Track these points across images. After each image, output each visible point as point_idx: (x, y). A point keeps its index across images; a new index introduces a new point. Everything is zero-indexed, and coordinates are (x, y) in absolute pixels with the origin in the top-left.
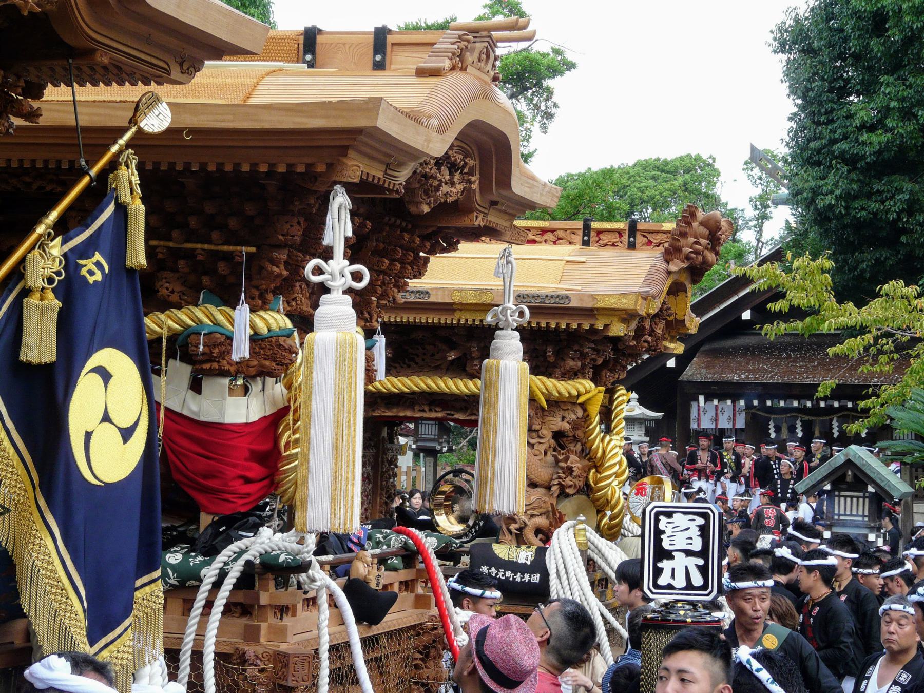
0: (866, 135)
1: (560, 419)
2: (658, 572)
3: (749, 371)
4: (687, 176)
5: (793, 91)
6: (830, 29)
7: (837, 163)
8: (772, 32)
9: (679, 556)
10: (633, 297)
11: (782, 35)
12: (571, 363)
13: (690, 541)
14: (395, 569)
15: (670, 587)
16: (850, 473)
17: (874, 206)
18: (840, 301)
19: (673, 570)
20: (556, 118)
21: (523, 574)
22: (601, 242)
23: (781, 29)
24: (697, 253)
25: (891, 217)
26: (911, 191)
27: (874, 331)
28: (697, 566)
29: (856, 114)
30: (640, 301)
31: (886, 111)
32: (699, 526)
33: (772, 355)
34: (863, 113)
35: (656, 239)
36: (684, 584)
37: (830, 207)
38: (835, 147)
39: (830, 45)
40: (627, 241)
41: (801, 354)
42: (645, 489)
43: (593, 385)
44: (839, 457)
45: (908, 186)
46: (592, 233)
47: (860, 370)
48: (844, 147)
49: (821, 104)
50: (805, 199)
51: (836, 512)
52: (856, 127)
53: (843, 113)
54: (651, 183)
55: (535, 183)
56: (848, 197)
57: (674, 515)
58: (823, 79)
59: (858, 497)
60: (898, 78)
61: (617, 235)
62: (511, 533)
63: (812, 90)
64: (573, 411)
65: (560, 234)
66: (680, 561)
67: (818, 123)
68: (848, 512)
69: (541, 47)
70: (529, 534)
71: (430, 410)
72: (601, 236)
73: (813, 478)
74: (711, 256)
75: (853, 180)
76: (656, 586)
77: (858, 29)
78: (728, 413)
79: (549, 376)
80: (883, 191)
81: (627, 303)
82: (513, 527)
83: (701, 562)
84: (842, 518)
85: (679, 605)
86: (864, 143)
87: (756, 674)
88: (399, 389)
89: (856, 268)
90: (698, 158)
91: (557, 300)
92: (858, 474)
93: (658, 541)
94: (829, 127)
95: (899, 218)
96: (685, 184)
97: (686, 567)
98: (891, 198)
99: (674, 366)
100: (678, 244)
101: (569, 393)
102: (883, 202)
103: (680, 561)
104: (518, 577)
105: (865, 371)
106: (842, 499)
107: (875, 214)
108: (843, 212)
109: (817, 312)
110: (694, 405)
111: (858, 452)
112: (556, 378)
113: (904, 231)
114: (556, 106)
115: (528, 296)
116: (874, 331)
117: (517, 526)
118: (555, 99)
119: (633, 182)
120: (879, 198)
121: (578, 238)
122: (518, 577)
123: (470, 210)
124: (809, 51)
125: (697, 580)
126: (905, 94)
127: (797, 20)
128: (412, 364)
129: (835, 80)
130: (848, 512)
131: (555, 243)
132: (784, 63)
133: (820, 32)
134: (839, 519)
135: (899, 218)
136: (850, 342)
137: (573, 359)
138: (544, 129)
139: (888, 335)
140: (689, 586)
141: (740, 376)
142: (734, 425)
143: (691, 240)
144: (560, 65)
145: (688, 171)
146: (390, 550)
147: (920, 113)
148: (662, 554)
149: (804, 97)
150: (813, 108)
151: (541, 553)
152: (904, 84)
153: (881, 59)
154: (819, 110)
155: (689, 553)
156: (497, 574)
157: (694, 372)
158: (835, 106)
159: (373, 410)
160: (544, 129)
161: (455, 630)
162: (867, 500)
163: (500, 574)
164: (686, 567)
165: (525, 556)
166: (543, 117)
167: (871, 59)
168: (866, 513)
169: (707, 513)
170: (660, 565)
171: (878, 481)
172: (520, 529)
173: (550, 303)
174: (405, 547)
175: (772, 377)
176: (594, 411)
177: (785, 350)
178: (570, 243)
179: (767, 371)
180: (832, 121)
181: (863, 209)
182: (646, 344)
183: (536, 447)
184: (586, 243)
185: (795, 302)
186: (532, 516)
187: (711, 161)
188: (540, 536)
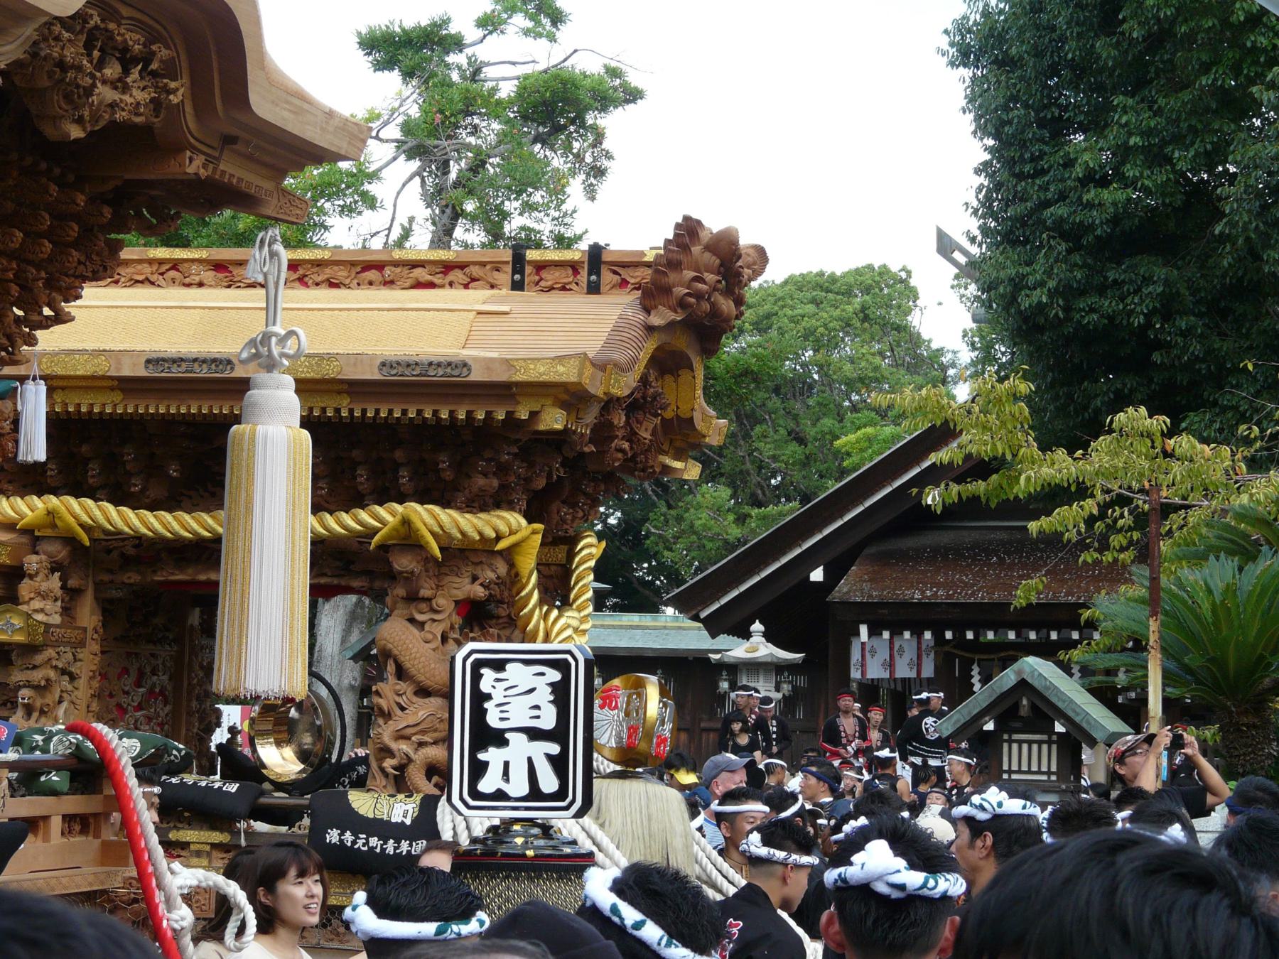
0: (1093, 192)
1: (468, 580)
2: (479, 769)
3: (938, 585)
4: (867, 298)
5: (982, 130)
6: (1037, 27)
7: (1049, 237)
8: (946, 32)
9: (517, 740)
10: (575, 363)
11: (963, 37)
12: (481, 481)
13: (536, 712)
14: (53, 792)
15: (500, 795)
16: (1025, 702)
17: (1108, 304)
18: (1044, 447)
19: (506, 764)
20: (610, 177)
21: (398, 841)
22: (543, 284)
23: (962, 27)
24: (699, 296)
25: (1137, 321)
26: (1166, 280)
27: (1100, 496)
28: (550, 758)
29: (1076, 159)
30: (589, 370)
31: (1123, 153)
32: (552, 684)
33: (974, 559)
34: (1086, 157)
35: (634, 276)
36: (524, 790)
37: (1040, 307)
38: (1047, 213)
39: (1038, 53)
40: (585, 280)
41: (1021, 557)
42: (617, 697)
43: (524, 522)
44: (1008, 678)
45: (1160, 272)
46: (528, 269)
47: (1081, 560)
48: (1060, 212)
49: (1023, 145)
50: (1002, 296)
51: (1005, 767)
52: (1079, 179)
53: (1058, 158)
54: (811, 308)
55: (306, 106)
56: (1067, 292)
57: (508, 667)
58: (1026, 106)
59: (1040, 743)
60: (1143, 101)
61: (570, 271)
62: (386, 775)
63: (1010, 122)
64: (491, 566)
65: (475, 271)
66: (519, 749)
67: (1021, 177)
68: (1025, 768)
70: (416, 776)
72: (544, 274)
73: (965, 712)
74: (727, 305)
75: (1076, 265)
76: (475, 794)
77: (1077, 24)
79: (445, 504)
80: (1123, 281)
81: (566, 373)
82: (389, 763)
83: (554, 749)
84: (1014, 777)
85: (517, 827)
86: (1090, 205)
87: (635, 933)
88: (195, 533)
89: (1086, 408)
90: (884, 271)
91: (449, 370)
92: (1039, 703)
93: (478, 713)
94: (1038, 182)
95: (1148, 325)
96: (864, 309)
97: (530, 759)
98: (1135, 292)
99: (821, 579)
100: (664, 280)
101: (480, 533)
102: (1122, 299)
103: (519, 749)
104: (390, 847)
105: (1090, 560)
107: (1111, 318)
108: (1061, 316)
109: (1010, 466)
111: (1037, 668)
112: (459, 509)
113: (1158, 345)
114: (609, 156)
115: (398, 363)
116: (1098, 493)
117: (394, 762)
118: (606, 145)
119: (783, 307)
120: (1117, 293)
121: (505, 277)
122: (390, 847)
123: (177, 148)
124: (1004, 63)
125: (549, 783)
126: (1152, 125)
127: (986, 14)
129: (1046, 107)
130: (1025, 768)
131: (466, 286)
132: (968, 82)
133: (1022, 31)
134: (1010, 779)
135: (1148, 325)
137: (485, 475)
138: (591, 193)
139: (1122, 501)
140: (535, 793)
141: (923, 593)
142: (919, 672)
143: (688, 274)
144: (615, 92)
145: (867, 290)
146: (46, 757)
147: (1176, 155)
148: (485, 736)
149: (996, 136)
150: (1013, 153)
151: (429, 806)
152: (1150, 108)
153: (1113, 69)
154: (1022, 156)
155: (534, 734)
156: (354, 843)
157: (854, 586)
158: (1046, 149)
159: (154, 572)
160: (591, 193)
161: (168, 901)
162: (1054, 747)
163: (360, 842)
164: (530, 759)
165: (402, 810)
166: (588, 175)
167: (1100, 71)
168: (1054, 769)
169: (566, 660)
170: (482, 756)
171: (1071, 714)
172: (401, 768)
173: (436, 376)
174: (78, 754)
175: (974, 592)
176: (528, 562)
177: (996, 553)
178: (492, 287)
179: (966, 584)
180: (1043, 172)
181: (1092, 310)
182: (620, 455)
183: (427, 627)
184: (517, 286)
185: (973, 449)
186: (421, 744)
187: (903, 275)
188: (435, 779)
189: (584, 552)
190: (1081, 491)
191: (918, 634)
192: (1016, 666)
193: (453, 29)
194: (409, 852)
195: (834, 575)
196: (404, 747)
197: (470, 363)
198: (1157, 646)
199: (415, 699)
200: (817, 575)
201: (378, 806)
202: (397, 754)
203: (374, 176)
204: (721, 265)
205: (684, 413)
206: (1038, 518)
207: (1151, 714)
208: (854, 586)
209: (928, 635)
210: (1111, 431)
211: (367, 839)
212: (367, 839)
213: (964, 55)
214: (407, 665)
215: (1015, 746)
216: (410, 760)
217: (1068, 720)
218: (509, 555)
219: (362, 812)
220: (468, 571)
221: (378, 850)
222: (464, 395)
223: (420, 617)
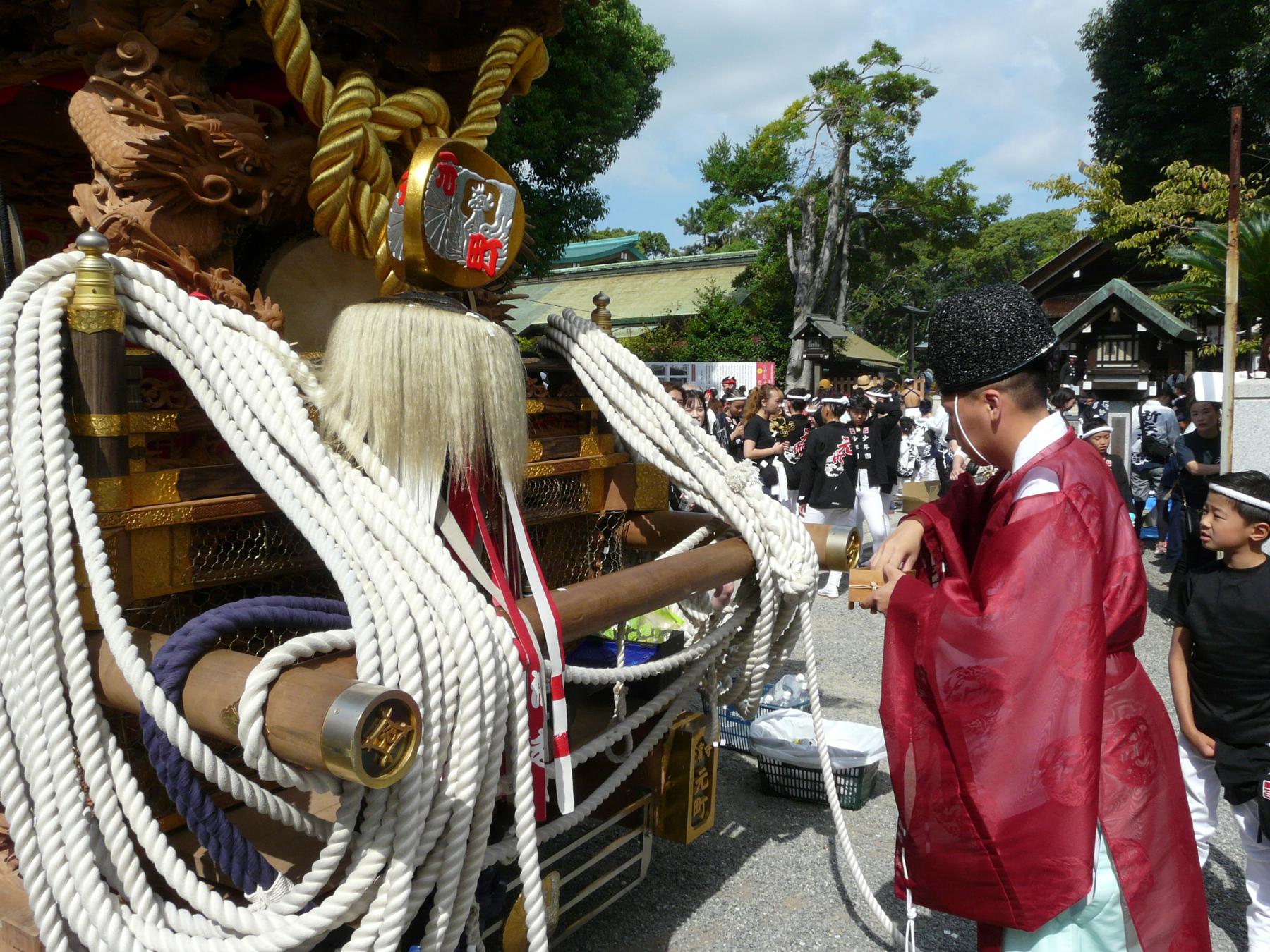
16: (1115, 310)
23: (1088, 28)
51: (1099, 359)
59: (1126, 341)
69: (904, 72)
114: (918, 114)
127: (1100, 20)
136: (1136, 237)
138: (911, 131)
162: (1137, 343)
168: (1136, 358)
171: (1151, 317)
190: (1150, 226)
192: (1108, 285)
193: (850, 68)
198: (1235, 244)
203: (804, 125)
207: (1228, 301)
210: (1165, 178)
217: (1146, 321)
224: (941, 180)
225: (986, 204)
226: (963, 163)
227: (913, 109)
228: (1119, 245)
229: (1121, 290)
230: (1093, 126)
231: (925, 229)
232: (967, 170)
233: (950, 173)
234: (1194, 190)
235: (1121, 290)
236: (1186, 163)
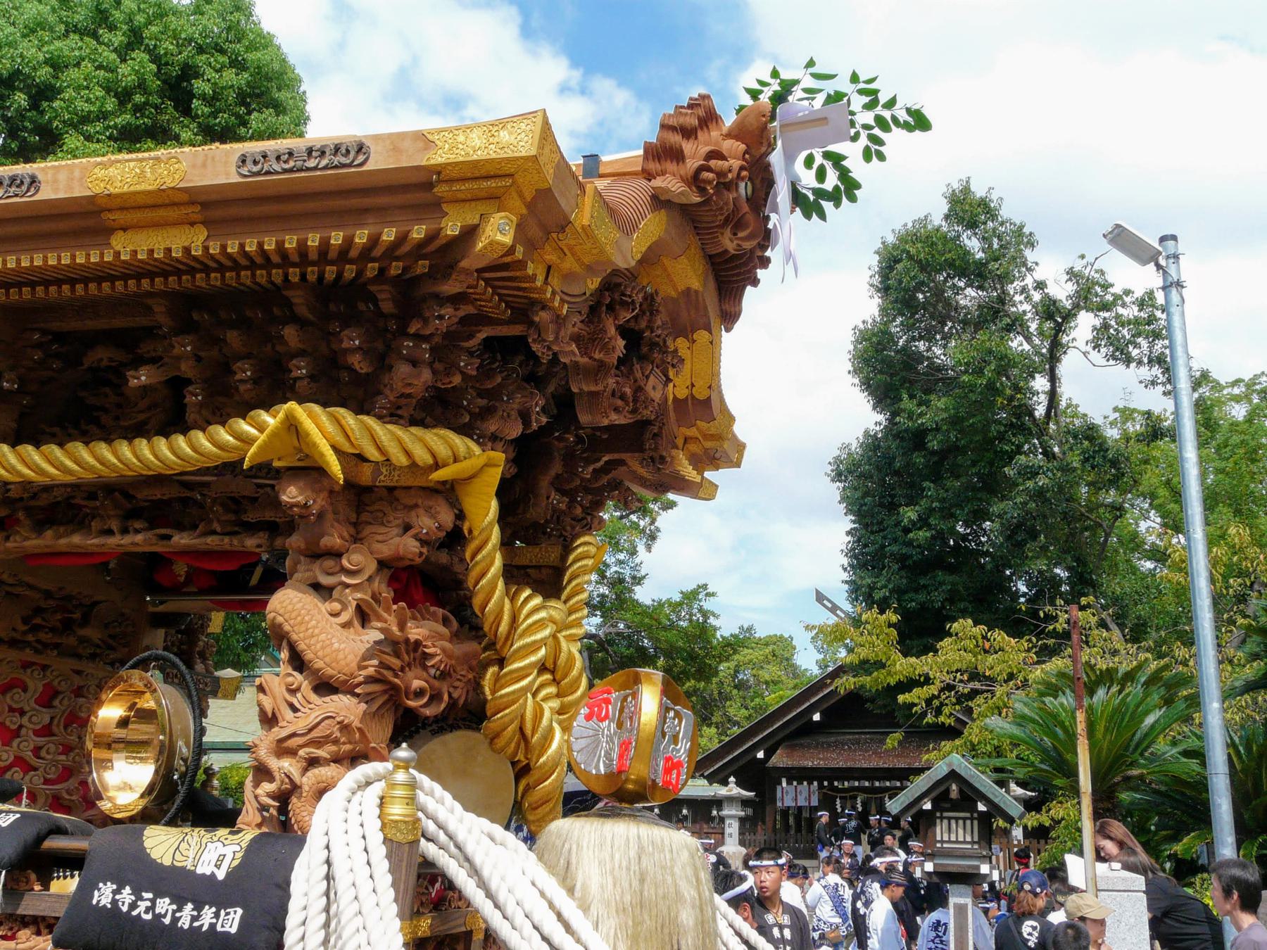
1: (395, 531)
16: (954, 787)
17: (922, 597)
21: (198, 908)
23: (837, 460)
51: (939, 838)
59: (964, 819)
64: (428, 510)
71: (125, 531)
78: (805, 794)
90: (781, 637)
95: (943, 607)
106: (945, 822)
110: (779, 788)
112: (380, 417)
114: (658, 530)
128: (93, 429)
135: (943, 607)
138: (649, 548)
139: (949, 688)
156: (133, 906)
157: (780, 759)
160: (649, 548)
162: (976, 822)
163: (143, 905)
168: (976, 839)
171: (991, 797)
183: (335, 594)
186: (313, 762)
189: (580, 550)
190: (927, 681)
191: (810, 783)
194: (213, 926)
195: (769, 754)
196: (287, 766)
197: (367, 143)
198: (1084, 734)
199: (313, 697)
200: (760, 755)
201: (184, 846)
202: (277, 775)
204: (746, 152)
205: (700, 394)
206: (910, 691)
207: (1083, 790)
208: (780, 759)
209: (815, 783)
210: (951, 635)
211: (153, 901)
212: (153, 901)
213: (838, 476)
214: (309, 656)
215: (945, 822)
216: (295, 788)
218: (449, 492)
219: (155, 855)
220: (397, 518)
221: (167, 921)
222: (365, 211)
223: (325, 580)
224: (680, 604)
225: (727, 634)
226: (705, 586)
227: (653, 522)
228: (901, 698)
229: (960, 765)
230: (845, 561)
231: (656, 657)
232: (708, 595)
233: (691, 597)
234: (978, 650)
235: (960, 765)
236: (970, 621)
